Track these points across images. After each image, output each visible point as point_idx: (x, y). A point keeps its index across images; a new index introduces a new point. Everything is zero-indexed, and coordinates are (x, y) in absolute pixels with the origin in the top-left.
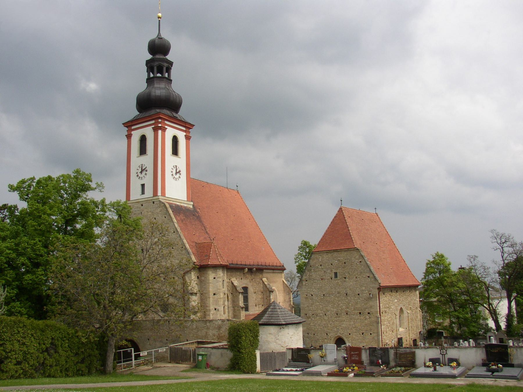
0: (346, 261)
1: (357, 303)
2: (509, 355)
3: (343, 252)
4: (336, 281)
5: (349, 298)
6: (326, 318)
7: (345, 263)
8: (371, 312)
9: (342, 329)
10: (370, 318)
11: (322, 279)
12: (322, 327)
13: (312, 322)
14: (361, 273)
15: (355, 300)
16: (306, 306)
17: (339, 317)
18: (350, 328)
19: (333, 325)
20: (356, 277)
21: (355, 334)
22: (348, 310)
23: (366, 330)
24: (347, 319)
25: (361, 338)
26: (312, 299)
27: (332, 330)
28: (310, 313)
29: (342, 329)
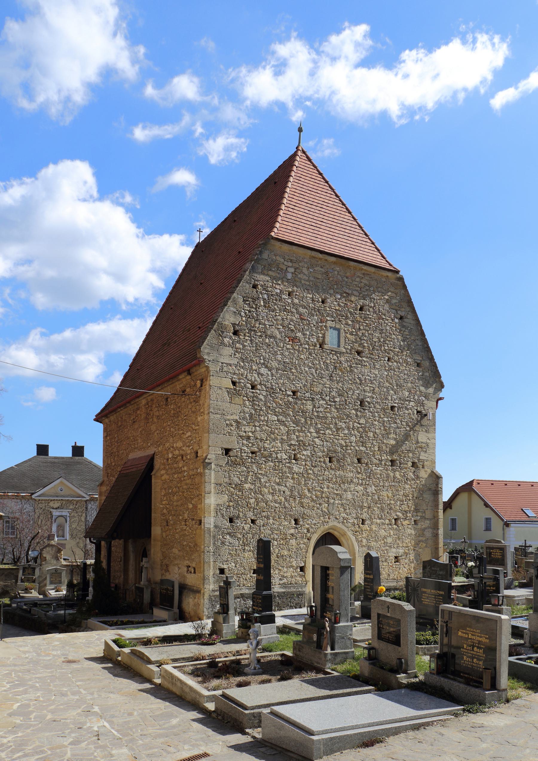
26: (253, 400)
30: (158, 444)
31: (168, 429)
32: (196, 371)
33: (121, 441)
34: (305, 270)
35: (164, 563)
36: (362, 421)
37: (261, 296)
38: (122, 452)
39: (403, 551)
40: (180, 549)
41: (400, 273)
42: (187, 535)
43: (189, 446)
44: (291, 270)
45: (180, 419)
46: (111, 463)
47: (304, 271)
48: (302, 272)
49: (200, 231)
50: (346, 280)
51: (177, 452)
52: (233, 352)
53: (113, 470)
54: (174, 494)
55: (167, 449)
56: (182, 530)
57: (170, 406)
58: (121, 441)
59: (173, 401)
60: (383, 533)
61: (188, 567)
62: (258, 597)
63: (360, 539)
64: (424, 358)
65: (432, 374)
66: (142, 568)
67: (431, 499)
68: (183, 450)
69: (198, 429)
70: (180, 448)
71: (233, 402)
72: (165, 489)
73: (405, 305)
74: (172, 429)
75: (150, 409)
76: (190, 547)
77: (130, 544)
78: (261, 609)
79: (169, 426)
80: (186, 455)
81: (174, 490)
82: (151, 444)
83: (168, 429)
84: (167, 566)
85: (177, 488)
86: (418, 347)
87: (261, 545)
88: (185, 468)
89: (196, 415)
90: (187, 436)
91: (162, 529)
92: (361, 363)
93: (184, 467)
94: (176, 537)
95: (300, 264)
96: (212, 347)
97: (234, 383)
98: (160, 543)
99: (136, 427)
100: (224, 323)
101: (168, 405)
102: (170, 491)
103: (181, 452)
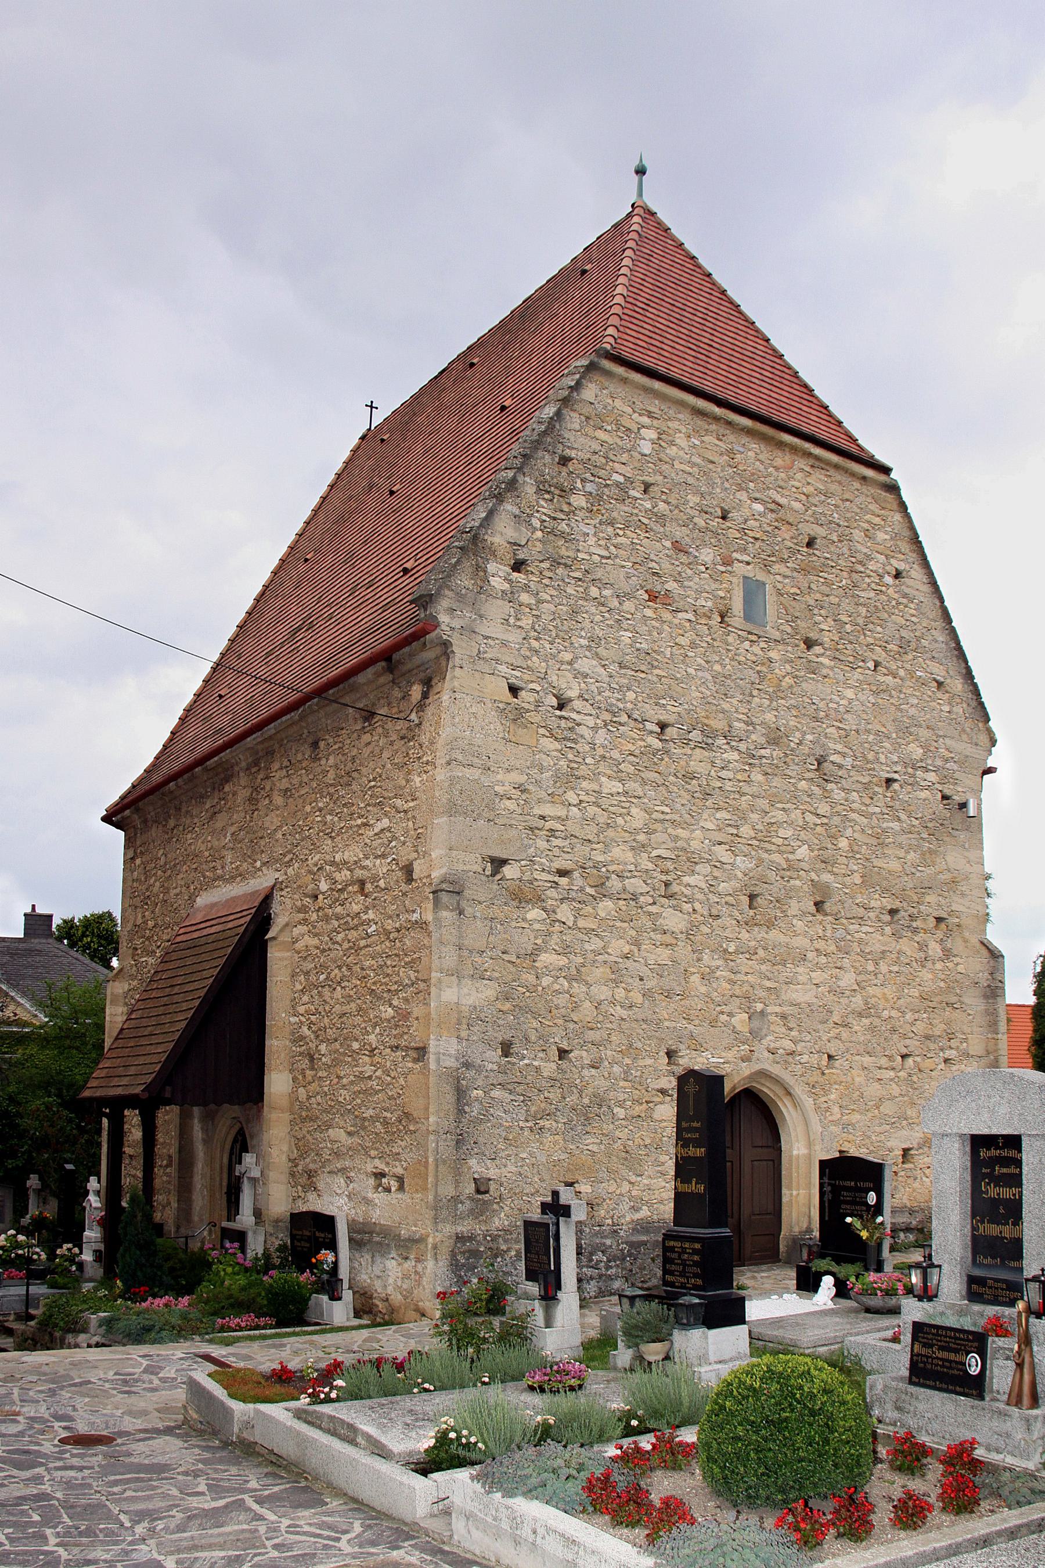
0: (821, 531)
1: (880, 840)
2: (103, 1193)
3: (801, 463)
4: (756, 649)
5: (838, 795)
6: (674, 920)
7: (810, 544)
8: (952, 913)
9: (784, 1017)
10: (948, 954)
11: (653, 597)
12: (637, 997)
13: (554, 941)
14: (904, 647)
15: (868, 816)
16: (505, 781)
17: (770, 925)
18: (836, 1018)
19: (726, 985)
20: (877, 664)
21: (867, 1060)
22: (826, 877)
23: (927, 1037)
24: (820, 945)
25: (895, 1090)
26: (568, 738)
27: (713, 1023)
28: (539, 852)
29: (784, 1017)
30: (287, 859)
31: (319, 819)
32: (411, 655)
33: (175, 866)
34: (681, 440)
35: (300, 1168)
36: (824, 809)
37: (579, 485)
38: (178, 891)
39: (922, 1136)
40: (350, 1129)
41: (893, 475)
42: (377, 1092)
43: (383, 856)
44: (652, 435)
45: (355, 787)
46: (145, 922)
47: (678, 441)
48: (672, 443)
49: (371, 407)
50: (775, 473)
51: (344, 875)
52: (512, 613)
53: (148, 939)
54: (332, 984)
55: (316, 869)
56: (361, 1078)
57: (323, 761)
58: (175, 866)
59: (336, 747)
60: (874, 1090)
61: (380, 1175)
62: (687, 1245)
63: (826, 1105)
64: (951, 673)
65: (970, 710)
66: (239, 1179)
67: (979, 1008)
68: (364, 868)
69: (414, 809)
70: (356, 862)
71: (514, 739)
72: (307, 973)
73: (905, 546)
74: (329, 818)
75: (261, 776)
76: (386, 1123)
77: (196, 1121)
78: (699, 1282)
79: (320, 810)
80: (375, 879)
81: (332, 975)
82: (264, 864)
83: (319, 819)
84: (310, 1174)
85: (344, 969)
86: (937, 645)
87: (691, 1088)
88: (371, 915)
89: (409, 773)
90: (376, 830)
91: (294, 1079)
92: (813, 669)
93: (366, 913)
94: (341, 1099)
95: (670, 424)
96: (460, 597)
97: (514, 690)
98: (286, 1117)
99: (219, 825)
100: (490, 539)
101: (319, 759)
102: (322, 977)
103: (359, 873)
